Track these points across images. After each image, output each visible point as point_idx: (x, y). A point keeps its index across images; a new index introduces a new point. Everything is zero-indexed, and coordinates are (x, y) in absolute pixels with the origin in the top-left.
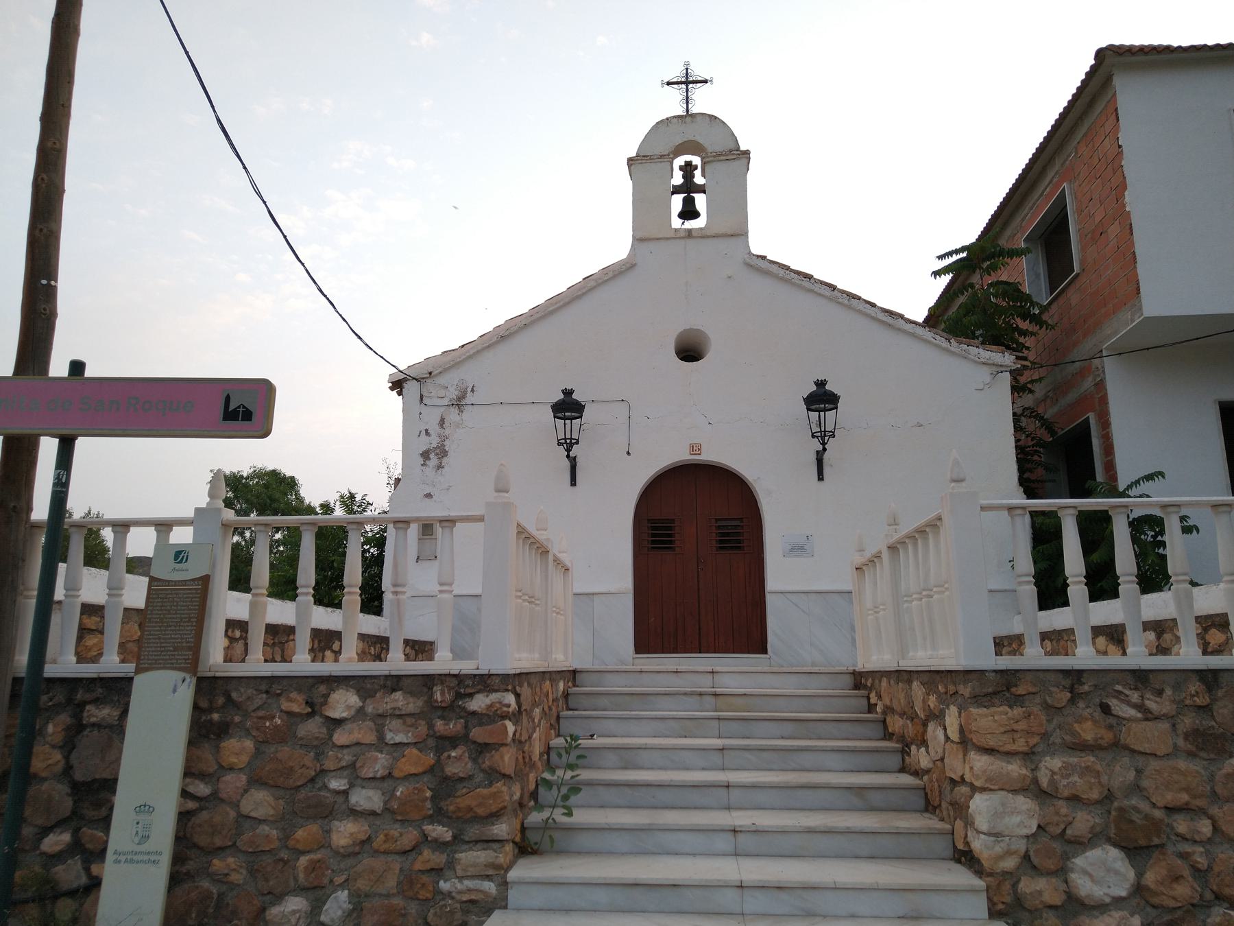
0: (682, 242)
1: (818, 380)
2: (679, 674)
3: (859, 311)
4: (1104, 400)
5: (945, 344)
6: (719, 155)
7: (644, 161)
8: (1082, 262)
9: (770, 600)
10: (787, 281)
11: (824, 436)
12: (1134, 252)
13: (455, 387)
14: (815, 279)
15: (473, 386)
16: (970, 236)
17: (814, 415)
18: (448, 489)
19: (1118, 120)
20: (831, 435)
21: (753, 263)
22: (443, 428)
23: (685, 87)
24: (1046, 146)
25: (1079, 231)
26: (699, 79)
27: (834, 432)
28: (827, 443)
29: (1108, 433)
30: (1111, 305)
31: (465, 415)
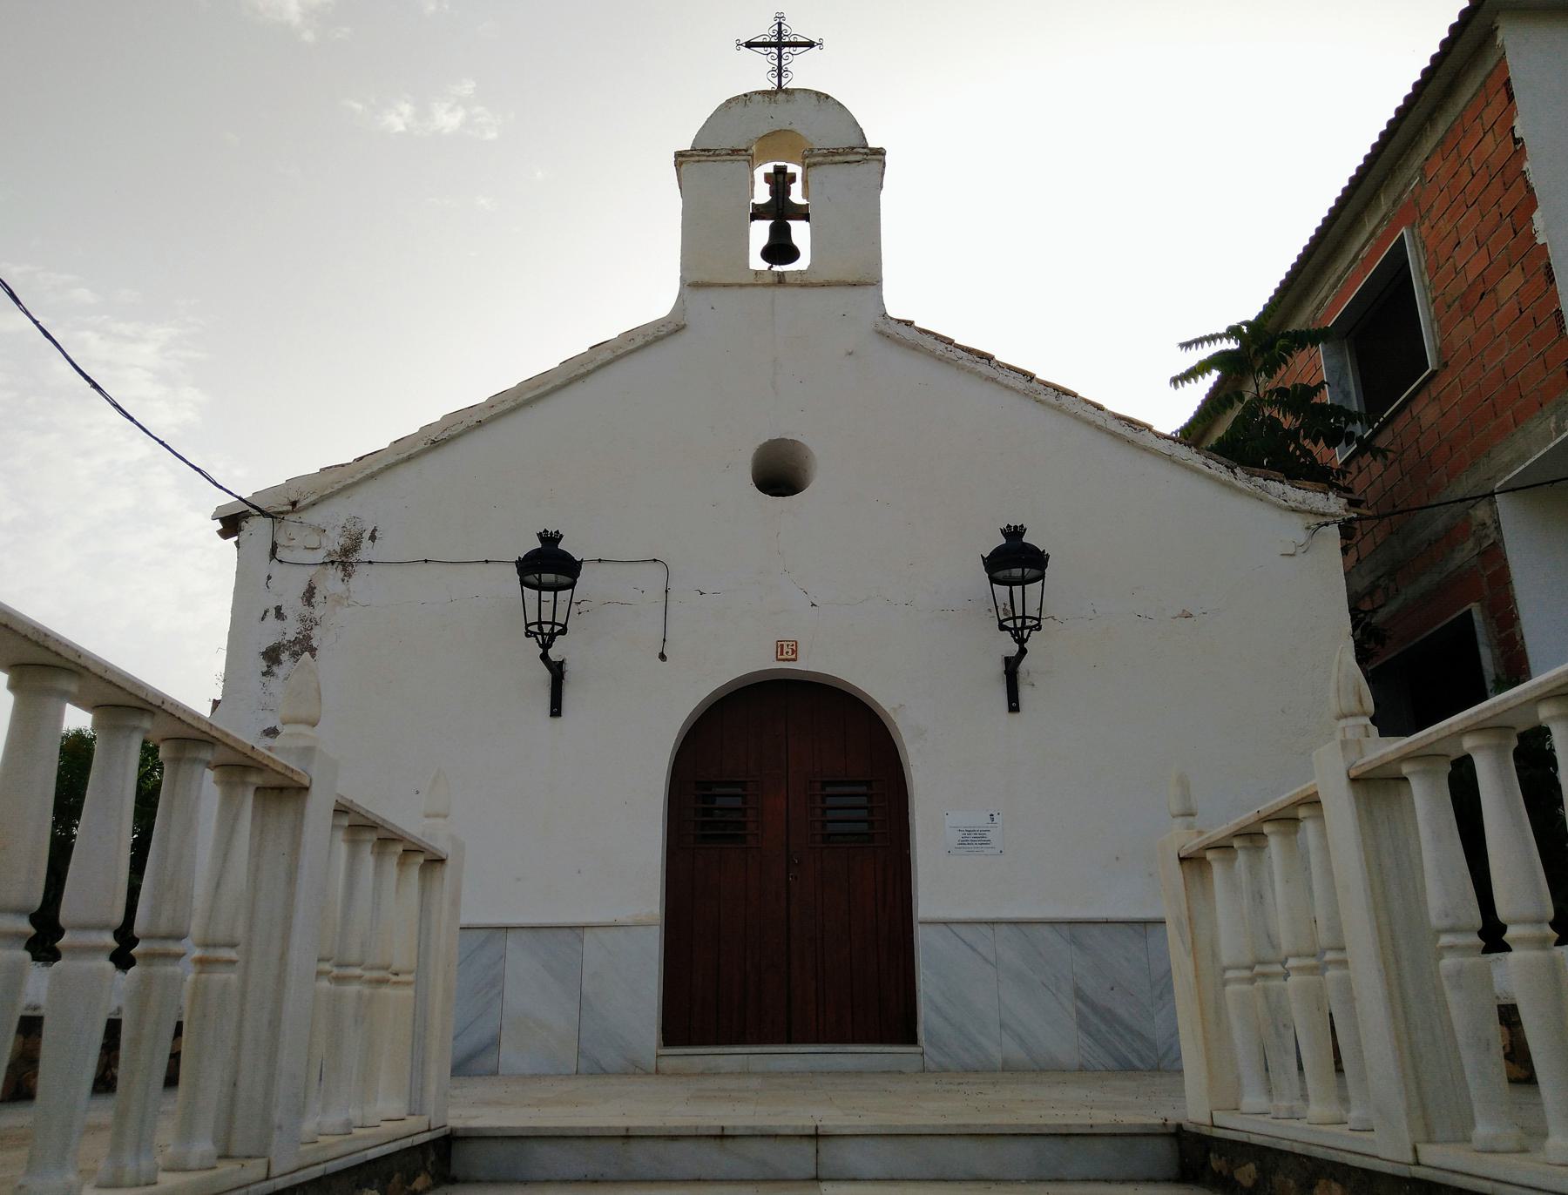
0: (769, 292)
1: (1009, 526)
2: (728, 1143)
3: (1076, 417)
4: (1502, 579)
5: (1226, 476)
6: (833, 154)
7: (704, 158)
8: (1440, 352)
9: (921, 935)
10: (948, 362)
11: (1020, 628)
12: (1559, 313)
14: (997, 361)
15: (375, 530)
16: (1250, 309)
17: (1002, 591)
19: (1511, 97)
20: (1034, 626)
21: (889, 331)
22: (310, 604)
23: (776, 52)
24: (1374, 163)
25: (1434, 301)
26: (800, 39)
27: (1039, 620)
28: (1026, 640)
29: (1513, 635)
30: (1509, 412)
31: (355, 582)
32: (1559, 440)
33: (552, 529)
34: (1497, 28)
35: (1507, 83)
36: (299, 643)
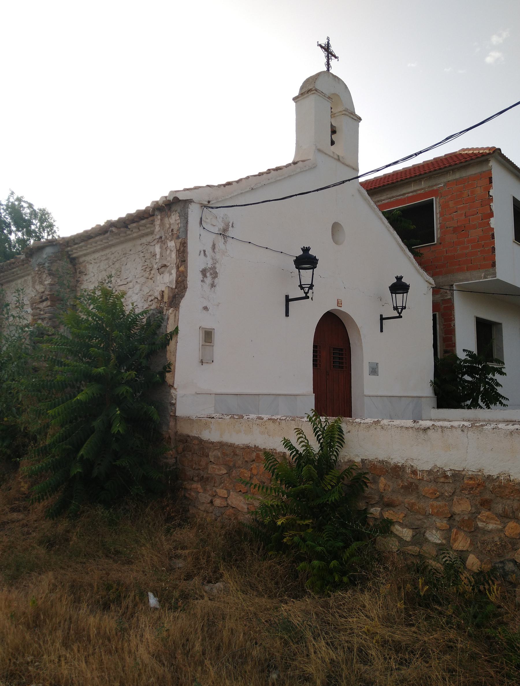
1: (304, 247)
13: (221, 219)
18: (218, 305)
32: (484, 280)
33: (399, 275)
34: (490, 160)
35: (491, 179)
36: (212, 269)
